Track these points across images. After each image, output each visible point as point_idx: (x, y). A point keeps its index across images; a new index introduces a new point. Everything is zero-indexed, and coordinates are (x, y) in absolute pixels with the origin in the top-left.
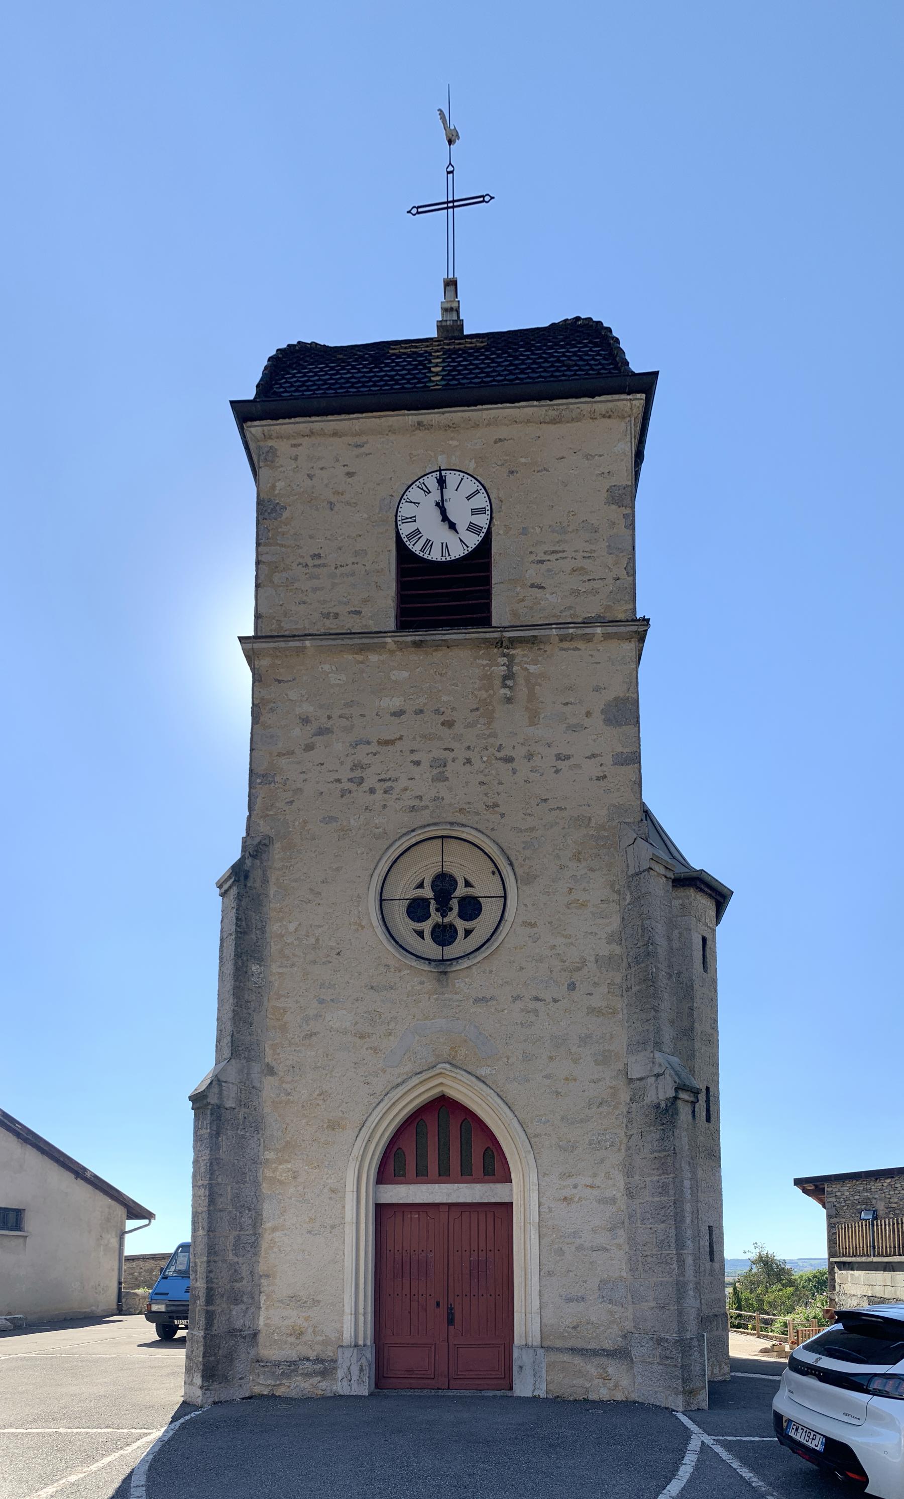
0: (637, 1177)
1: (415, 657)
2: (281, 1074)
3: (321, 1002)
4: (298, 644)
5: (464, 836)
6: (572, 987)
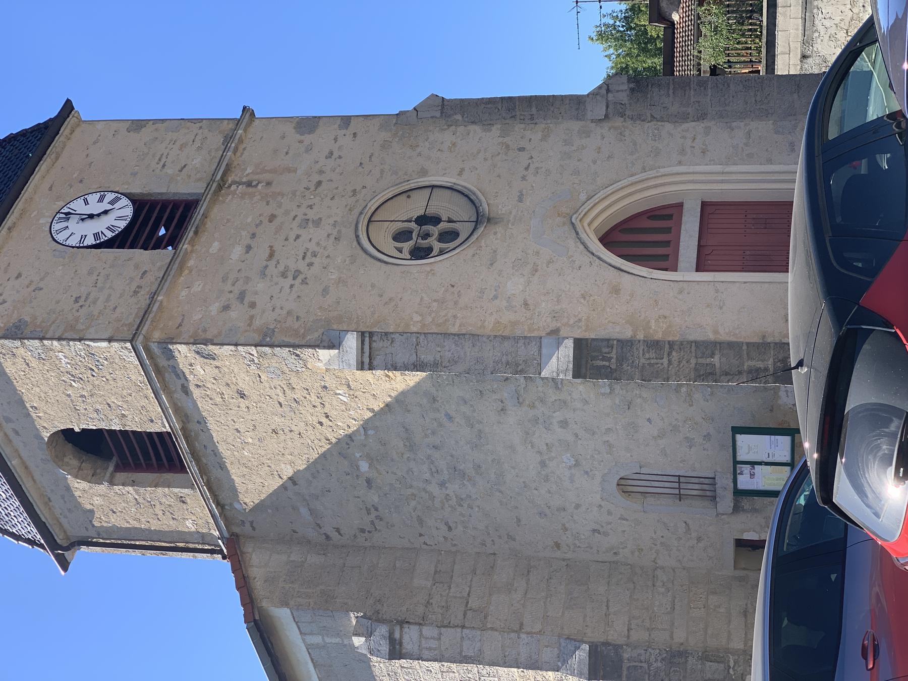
0: (690, 110)
1: (204, 238)
2: (559, 325)
3: (496, 297)
4: (157, 305)
5: (373, 209)
6: (522, 149)
